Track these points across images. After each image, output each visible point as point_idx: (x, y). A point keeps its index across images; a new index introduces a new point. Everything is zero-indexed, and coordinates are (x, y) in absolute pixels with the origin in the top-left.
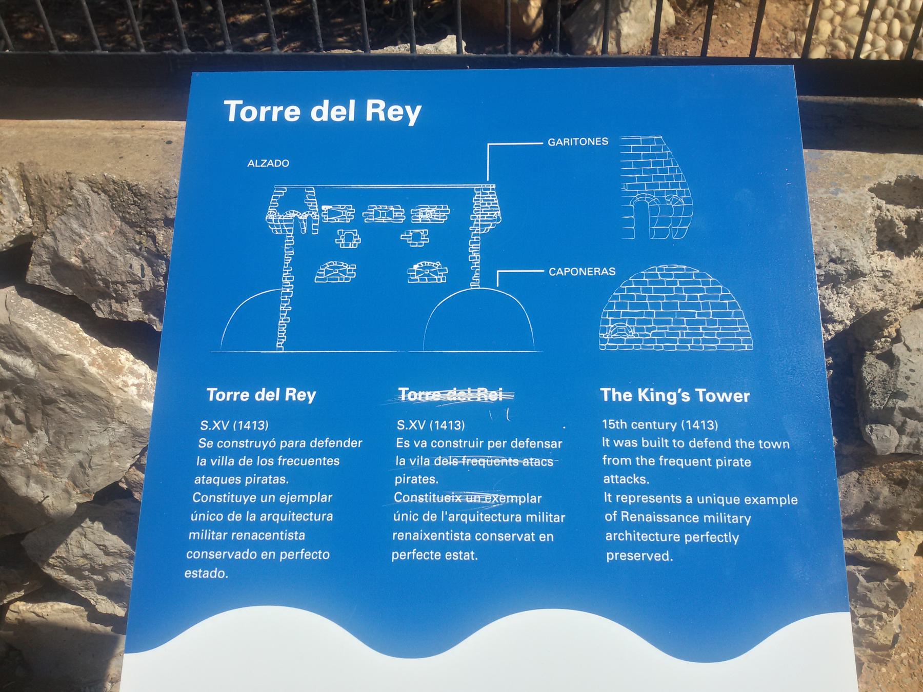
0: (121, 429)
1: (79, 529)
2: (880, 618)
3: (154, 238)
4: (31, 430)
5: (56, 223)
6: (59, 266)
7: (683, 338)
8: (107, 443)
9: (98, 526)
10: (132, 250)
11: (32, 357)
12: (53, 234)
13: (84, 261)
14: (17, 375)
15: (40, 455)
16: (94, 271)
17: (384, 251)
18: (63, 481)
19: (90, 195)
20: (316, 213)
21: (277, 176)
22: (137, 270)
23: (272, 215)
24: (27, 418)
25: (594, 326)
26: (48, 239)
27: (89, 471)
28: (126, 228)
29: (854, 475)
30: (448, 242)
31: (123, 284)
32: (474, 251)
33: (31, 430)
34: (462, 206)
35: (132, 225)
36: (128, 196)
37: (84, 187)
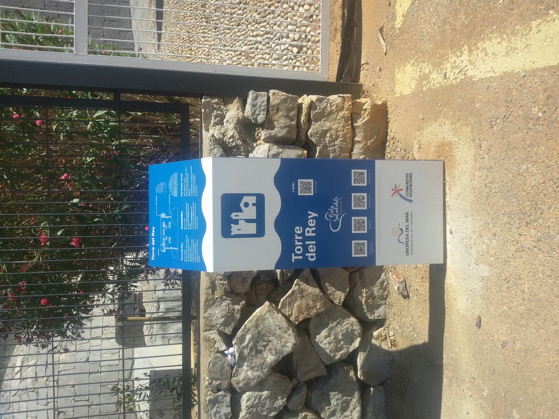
0: (268, 315)
1: (319, 343)
2: (331, 103)
3: (217, 298)
4: (270, 341)
5: (214, 323)
6: (225, 324)
7: (176, 183)
8: (272, 320)
9: (318, 337)
10: (220, 304)
11: (246, 335)
12: (217, 324)
13: (223, 317)
14: (251, 340)
15: (278, 341)
16: (226, 315)
17: (168, 233)
18: (286, 335)
19: (208, 312)
20: (163, 244)
21: (160, 250)
22: (225, 304)
23: (164, 251)
24: (266, 341)
25: (175, 197)
26: (218, 326)
27: (281, 326)
28: (215, 305)
29: (275, 123)
30: (167, 221)
31: (229, 308)
32: (168, 217)
33: (270, 341)
34: (164, 219)
35: (214, 303)
36: (207, 303)
37: (206, 314)
